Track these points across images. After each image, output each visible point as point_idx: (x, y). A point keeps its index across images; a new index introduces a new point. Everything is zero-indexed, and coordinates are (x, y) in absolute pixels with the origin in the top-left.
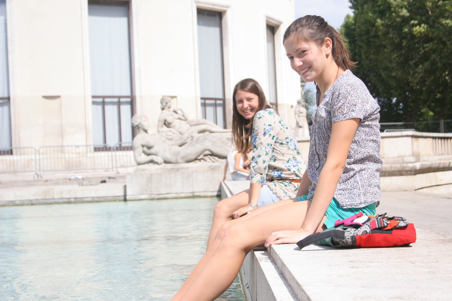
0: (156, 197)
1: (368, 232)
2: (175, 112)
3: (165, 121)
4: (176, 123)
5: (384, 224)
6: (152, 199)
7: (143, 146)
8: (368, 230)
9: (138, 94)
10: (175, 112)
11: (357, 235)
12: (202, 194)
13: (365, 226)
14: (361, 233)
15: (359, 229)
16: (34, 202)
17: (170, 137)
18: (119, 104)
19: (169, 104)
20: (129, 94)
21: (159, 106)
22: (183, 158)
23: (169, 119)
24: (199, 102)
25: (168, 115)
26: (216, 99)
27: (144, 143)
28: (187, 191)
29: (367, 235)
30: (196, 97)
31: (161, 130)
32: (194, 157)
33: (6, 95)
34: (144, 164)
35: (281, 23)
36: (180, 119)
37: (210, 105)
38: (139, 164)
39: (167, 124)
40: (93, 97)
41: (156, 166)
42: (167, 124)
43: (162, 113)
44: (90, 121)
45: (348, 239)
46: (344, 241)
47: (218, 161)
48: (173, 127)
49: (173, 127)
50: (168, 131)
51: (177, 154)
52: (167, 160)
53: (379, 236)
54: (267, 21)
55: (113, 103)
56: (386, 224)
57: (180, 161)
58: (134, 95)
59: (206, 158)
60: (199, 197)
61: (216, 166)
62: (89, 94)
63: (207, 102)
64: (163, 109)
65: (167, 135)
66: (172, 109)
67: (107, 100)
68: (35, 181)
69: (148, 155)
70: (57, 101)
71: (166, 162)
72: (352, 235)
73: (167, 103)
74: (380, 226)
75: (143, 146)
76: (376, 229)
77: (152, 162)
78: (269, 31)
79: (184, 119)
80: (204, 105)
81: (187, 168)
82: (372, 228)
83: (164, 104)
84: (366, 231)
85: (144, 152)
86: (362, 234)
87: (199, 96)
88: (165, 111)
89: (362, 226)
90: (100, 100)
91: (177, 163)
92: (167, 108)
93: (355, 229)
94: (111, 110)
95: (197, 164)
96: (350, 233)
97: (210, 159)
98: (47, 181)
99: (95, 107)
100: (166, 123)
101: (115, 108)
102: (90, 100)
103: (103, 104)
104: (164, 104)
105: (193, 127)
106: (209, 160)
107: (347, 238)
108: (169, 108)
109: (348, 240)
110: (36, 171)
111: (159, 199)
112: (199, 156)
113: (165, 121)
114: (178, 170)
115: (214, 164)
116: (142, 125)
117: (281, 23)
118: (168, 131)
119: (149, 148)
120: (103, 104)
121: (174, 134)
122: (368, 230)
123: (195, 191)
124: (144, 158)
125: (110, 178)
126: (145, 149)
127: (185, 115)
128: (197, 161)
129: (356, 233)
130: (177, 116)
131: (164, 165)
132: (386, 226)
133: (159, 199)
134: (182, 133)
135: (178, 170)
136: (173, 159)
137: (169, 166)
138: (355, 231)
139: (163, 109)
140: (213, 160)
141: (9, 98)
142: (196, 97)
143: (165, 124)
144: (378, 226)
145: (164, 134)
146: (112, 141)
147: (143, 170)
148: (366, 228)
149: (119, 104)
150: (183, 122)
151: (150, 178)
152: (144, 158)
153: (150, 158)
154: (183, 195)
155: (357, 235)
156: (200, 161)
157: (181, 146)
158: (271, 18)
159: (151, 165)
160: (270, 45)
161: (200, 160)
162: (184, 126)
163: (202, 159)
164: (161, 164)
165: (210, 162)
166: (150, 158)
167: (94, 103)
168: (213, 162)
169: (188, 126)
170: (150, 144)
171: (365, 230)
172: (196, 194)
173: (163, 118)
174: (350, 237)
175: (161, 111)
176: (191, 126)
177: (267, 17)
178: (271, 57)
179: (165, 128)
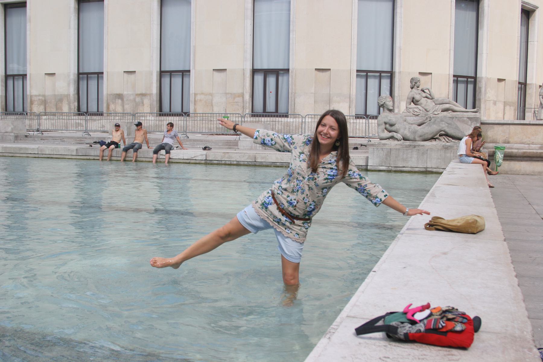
0: (394, 169)
2: (423, 91)
3: (413, 98)
4: (423, 101)
5: (439, 326)
6: (389, 171)
7: (386, 123)
8: (423, 329)
10: (423, 91)
11: (410, 333)
12: (434, 170)
17: (416, 114)
21: (409, 84)
22: (421, 136)
23: (417, 97)
24: (452, 79)
26: (467, 77)
27: (386, 120)
30: (449, 75)
31: (410, 106)
32: (430, 136)
34: (386, 139)
35: (537, 8)
36: (426, 97)
37: (462, 82)
39: (414, 101)
40: (358, 71)
42: (414, 101)
43: (411, 91)
44: (354, 92)
47: (451, 141)
48: (420, 105)
49: (420, 105)
51: (415, 132)
54: (522, 5)
55: (375, 77)
56: (440, 326)
57: (417, 139)
59: (441, 138)
61: (450, 146)
62: (355, 68)
63: (459, 79)
64: (412, 88)
65: (414, 111)
69: (390, 132)
70: (328, 73)
71: (405, 139)
72: (405, 332)
73: (416, 83)
76: (431, 329)
77: (392, 138)
78: (524, 15)
79: (430, 97)
80: (456, 82)
81: (423, 146)
84: (420, 330)
86: (415, 333)
87: (452, 73)
88: (413, 90)
91: (415, 140)
92: (415, 87)
95: (434, 143)
96: (407, 328)
97: (444, 139)
99: (359, 79)
102: (355, 73)
106: (444, 140)
108: (418, 87)
113: (413, 98)
114: (415, 147)
115: (448, 144)
116: (387, 105)
117: (537, 8)
119: (392, 125)
121: (420, 111)
122: (423, 329)
125: (362, 145)
126: (388, 126)
127: (432, 94)
130: (424, 95)
131: (403, 141)
132: (441, 329)
134: (428, 110)
135: (415, 147)
137: (408, 143)
139: (412, 88)
140: (447, 140)
142: (449, 75)
143: (413, 101)
145: (411, 110)
146: (372, 110)
147: (384, 144)
148: (421, 327)
150: (429, 101)
154: (417, 169)
156: (436, 140)
157: (419, 125)
158: (527, 3)
160: (524, 29)
162: (430, 104)
163: (437, 138)
164: (400, 140)
165: (443, 142)
168: (447, 142)
169: (434, 104)
175: (411, 90)
177: (523, 2)
178: (524, 40)
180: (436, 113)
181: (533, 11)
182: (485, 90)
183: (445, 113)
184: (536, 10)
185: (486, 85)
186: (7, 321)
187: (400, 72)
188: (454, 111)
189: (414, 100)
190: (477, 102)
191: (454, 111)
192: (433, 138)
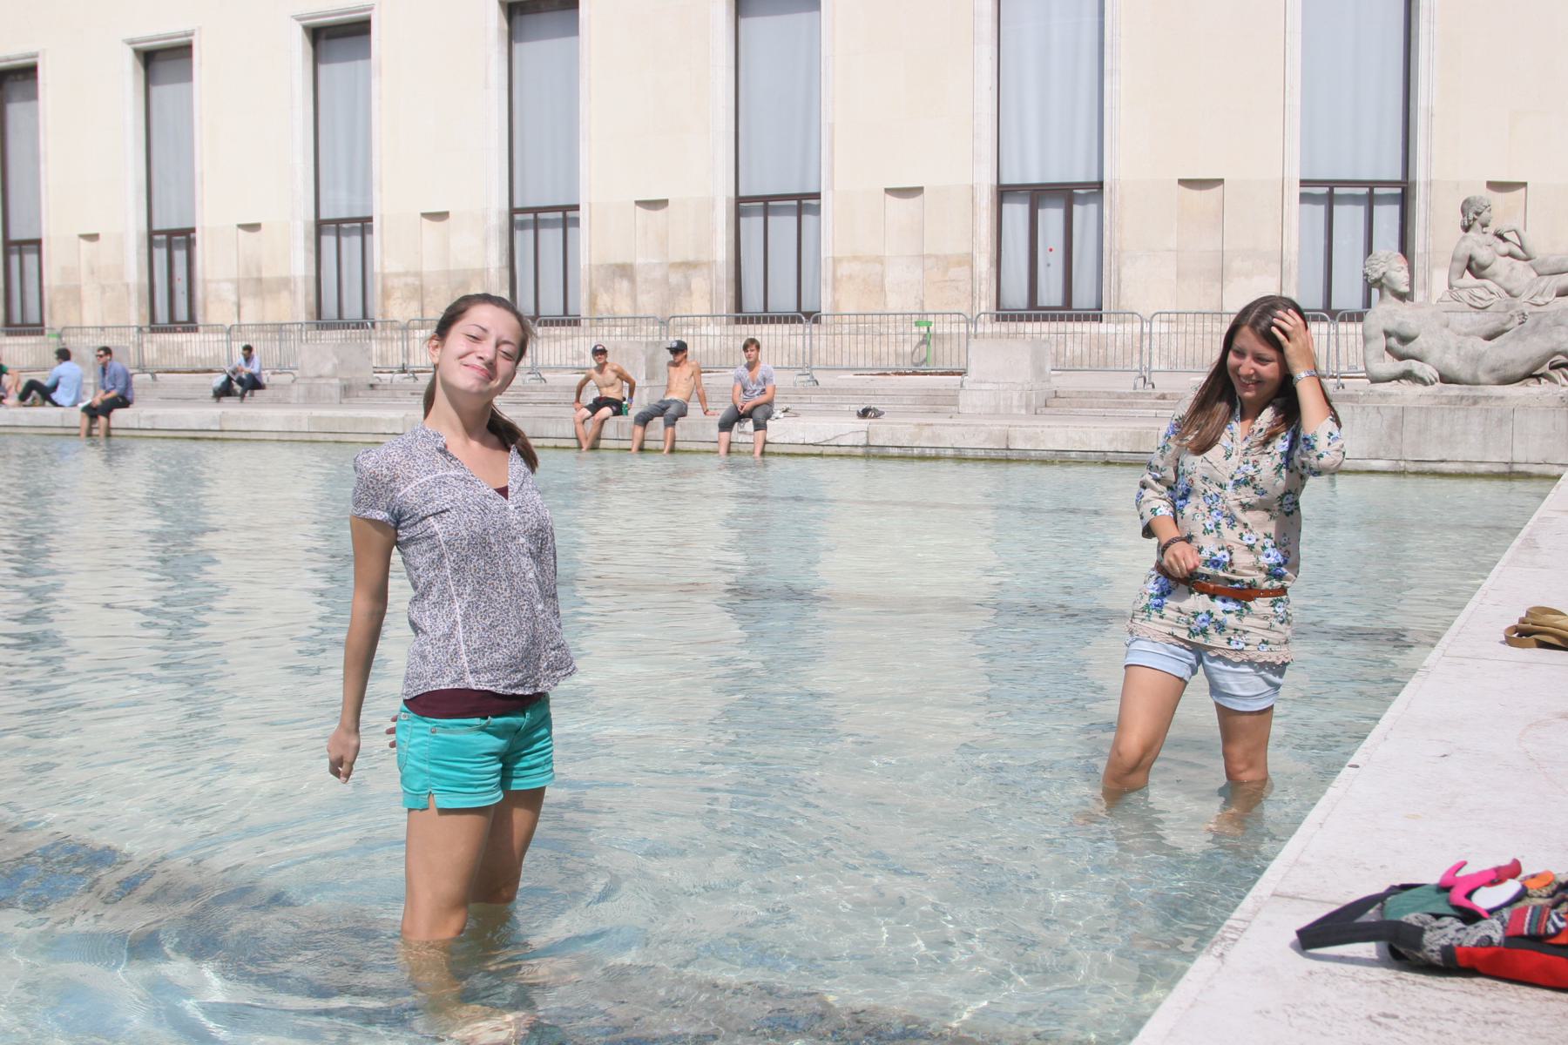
0: (1413, 467)
1: (1494, 941)
3: (1471, 259)
4: (1501, 266)
5: (1546, 927)
7: (1388, 334)
8: (1497, 936)
9: (1420, 175)
11: (1460, 945)
12: (1535, 469)
13: (1495, 922)
14: (1473, 943)
15: (1471, 928)
16: (1110, 457)
18: (1371, 201)
19: (1485, 214)
20: (1398, 177)
22: (1493, 370)
23: (1483, 255)
25: (1480, 245)
27: (1391, 326)
28: (1495, 458)
29: (1489, 950)
31: (1461, 282)
32: (1522, 370)
33: (1094, 179)
34: (1389, 380)
36: (1511, 255)
38: (1375, 380)
39: (1475, 268)
40: (1304, 183)
41: (1420, 388)
42: (1475, 268)
43: (1463, 238)
45: (1432, 951)
46: (1420, 955)
50: (1477, 287)
51: (1477, 359)
52: (1447, 372)
53: (1534, 959)
55: (1354, 199)
56: (1552, 930)
57: (1483, 377)
58: (1411, 179)
60: (1527, 476)
62: (1295, 176)
64: (1467, 229)
66: (1491, 229)
67: (1338, 191)
68: (1136, 395)
69: (1401, 357)
70: (1217, 190)
71: (1445, 379)
72: (1444, 942)
73: (1478, 214)
74: (1533, 931)
75: (1388, 334)
76: (1522, 936)
77: (1408, 376)
79: (1522, 255)
82: (1509, 933)
83: (1471, 216)
84: (1490, 938)
85: (1388, 349)
86: (1475, 946)
88: (1471, 233)
89: (1485, 919)
90: (1324, 190)
92: (1477, 225)
93: (1460, 925)
94: (1349, 218)
95: (1533, 388)
98: (1163, 397)
99: (1308, 207)
100: (1474, 265)
101: (1360, 211)
102: (1295, 191)
103: (1330, 201)
104: (1471, 216)
105: (1547, 278)
107: (1429, 948)
108: (1484, 225)
109: (1430, 954)
110: (1141, 371)
111: (1418, 473)
112: (1541, 365)
113: (1471, 259)
114: (1475, 401)
116: (1389, 280)
118: (1477, 287)
119: (1405, 340)
120: (1330, 201)
121: (1493, 296)
122: (1497, 936)
123: (1515, 460)
124: (1391, 366)
126: (1393, 341)
127: (1527, 245)
128: (1531, 381)
129: (1459, 939)
130: (1504, 247)
131: (1439, 384)
133: (1418, 473)
134: (1515, 292)
135: (1475, 401)
136: (1463, 371)
137: (1454, 390)
138: (1458, 930)
139: (1467, 229)
141: (1100, 185)
143: (1469, 268)
144: (1529, 930)
145: (1464, 294)
147: (1384, 396)
148: (1494, 930)
149: (1371, 201)
150: (1519, 264)
151: (1399, 419)
152: (1391, 366)
153: (1402, 366)
154: (1482, 468)
155: (1460, 945)
159: (1406, 387)
161: (1537, 377)
162: (1521, 275)
164: (1432, 383)
166: (1402, 366)
167: (1304, 198)
169: (1534, 275)
170: (1408, 331)
171: (1488, 932)
172: (1517, 468)
173: (1464, 252)
174: (1437, 948)
175: (1462, 233)
176: (1539, 275)
179: (1468, 278)
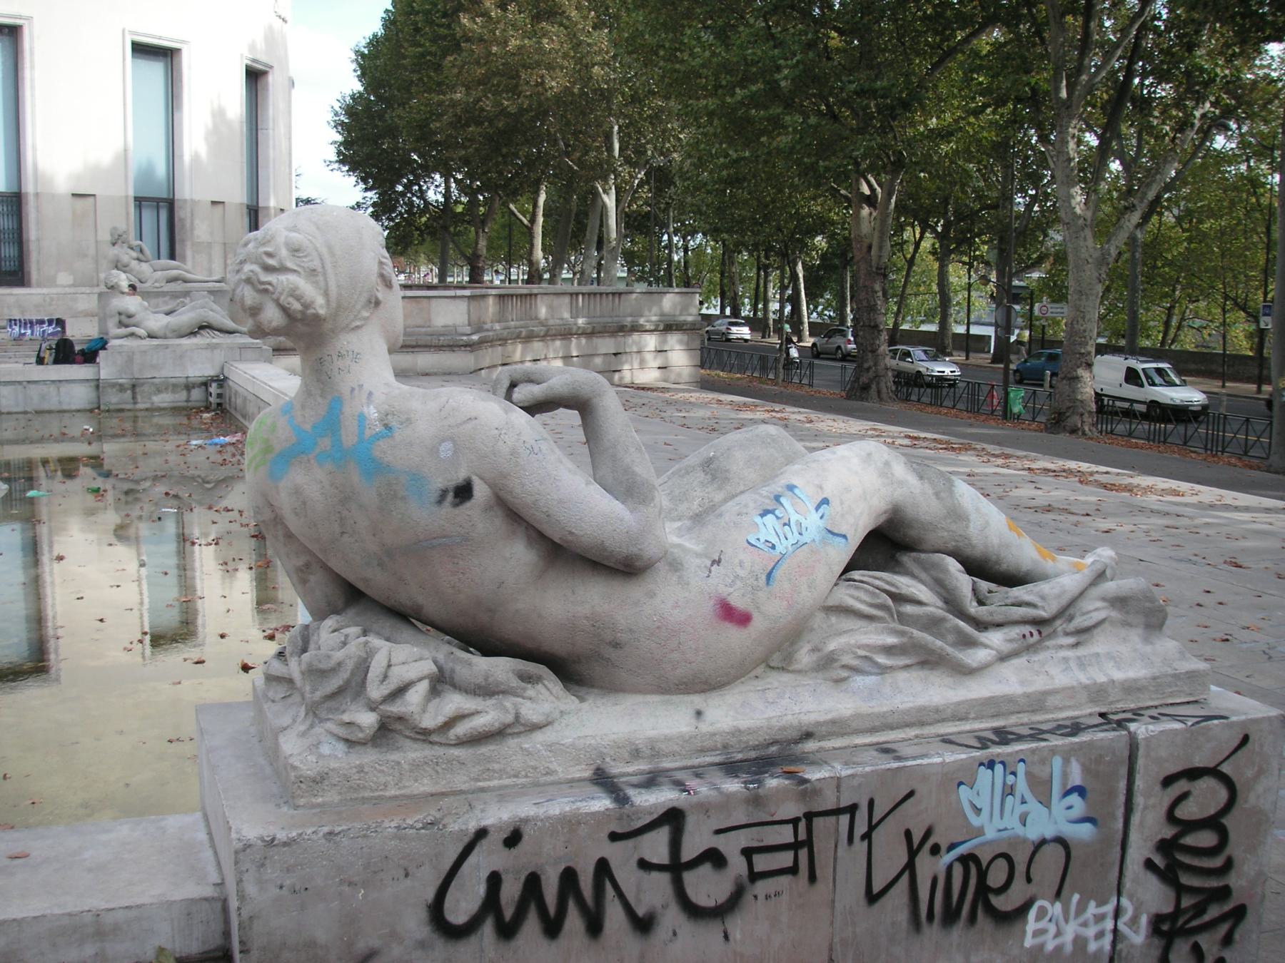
7: (120, 314)
32: (189, 331)
59: (202, 332)
71: (151, 336)
88: (116, 247)
113: (118, 261)
115: (214, 341)
117: (271, 67)
137: (155, 342)
180: (157, 285)
181: (264, 73)
182: (192, 223)
183: (172, 284)
184: (702, 366)
185: (192, 215)
186: (698, 561)
187: (37, 195)
188: (186, 281)
189: (119, 265)
190: (178, 247)
191: (186, 281)
192: (193, 334)
